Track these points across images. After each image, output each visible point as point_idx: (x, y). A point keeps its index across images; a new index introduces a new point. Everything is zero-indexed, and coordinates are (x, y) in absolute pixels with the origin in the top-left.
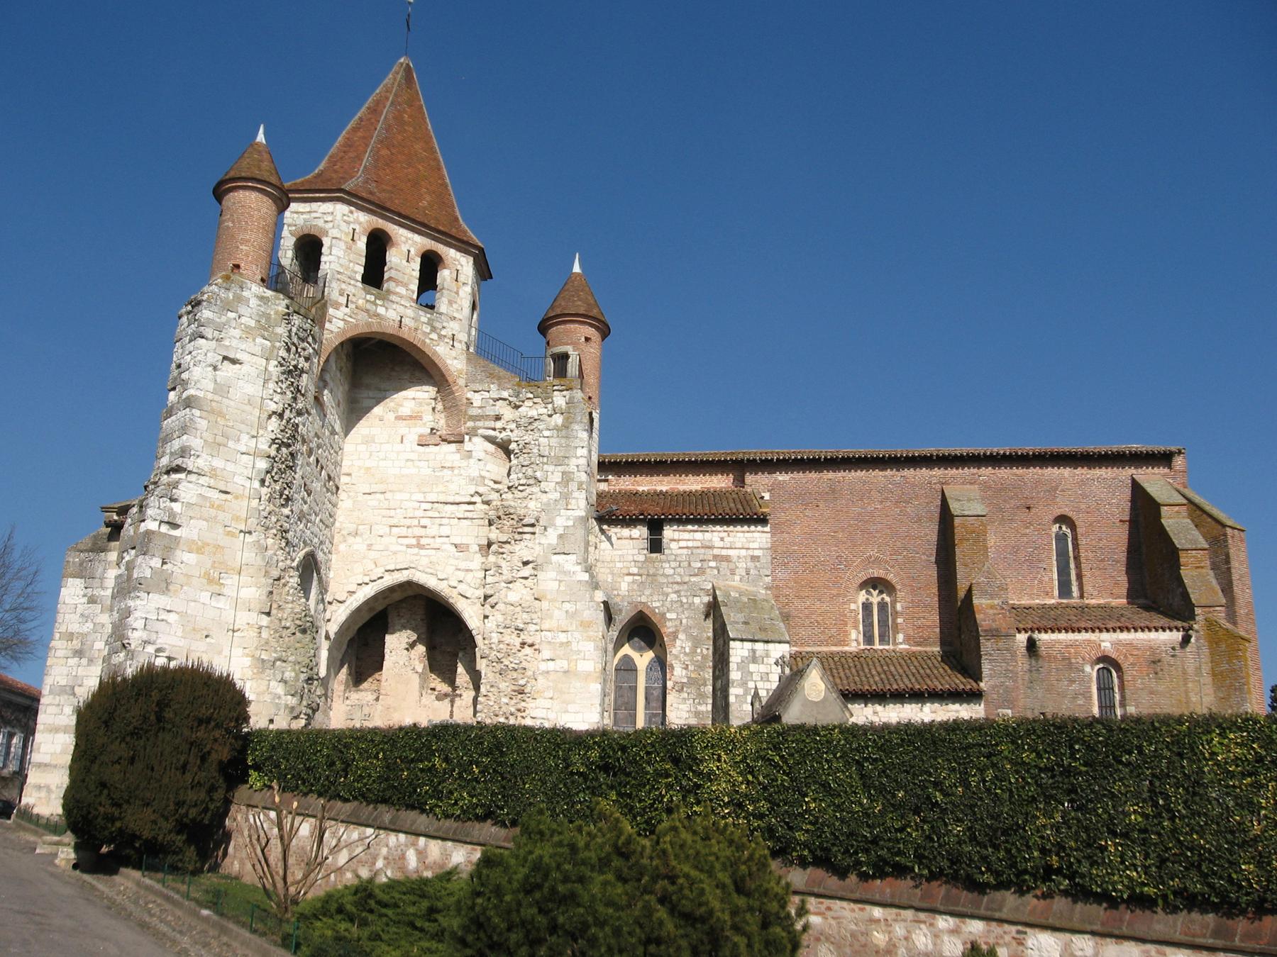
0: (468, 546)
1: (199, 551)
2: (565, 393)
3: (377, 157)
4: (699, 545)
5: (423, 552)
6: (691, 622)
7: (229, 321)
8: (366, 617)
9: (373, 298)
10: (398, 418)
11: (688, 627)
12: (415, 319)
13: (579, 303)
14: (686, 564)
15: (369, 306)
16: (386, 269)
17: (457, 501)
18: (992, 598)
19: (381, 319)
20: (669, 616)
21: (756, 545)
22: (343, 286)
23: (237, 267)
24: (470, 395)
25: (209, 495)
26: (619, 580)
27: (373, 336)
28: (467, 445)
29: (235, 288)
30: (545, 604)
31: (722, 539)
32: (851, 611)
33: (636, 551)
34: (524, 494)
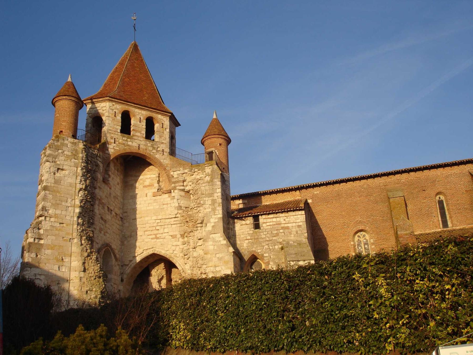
0: (176, 235)
1: (52, 248)
2: (210, 167)
3: (122, 80)
4: (275, 223)
5: (158, 240)
6: (274, 257)
7: (58, 154)
8: (140, 270)
9: (126, 138)
10: (145, 187)
11: (274, 259)
12: (146, 145)
13: (216, 130)
14: (270, 232)
15: (124, 142)
16: (131, 126)
17: (170, 217)
18: (406, 231)
19: (130, 147)
20: (265, 255)
21: (299, 221)
22: (112, 135)
23: (62, 131)
24: (172, 173)
25: (55, 225)
26: (243, 242)
27: (130, 154)
28: (173, 194)
29: (61, 141)
30: (209, 256)
31: (285, 220)
32: (352, 245)
33: (249, 230)
34: (197, 211)
